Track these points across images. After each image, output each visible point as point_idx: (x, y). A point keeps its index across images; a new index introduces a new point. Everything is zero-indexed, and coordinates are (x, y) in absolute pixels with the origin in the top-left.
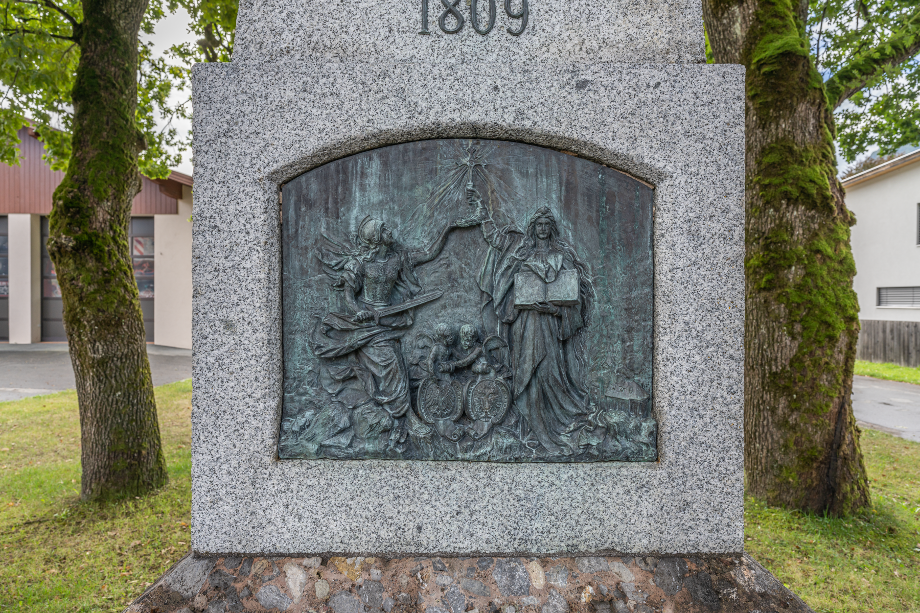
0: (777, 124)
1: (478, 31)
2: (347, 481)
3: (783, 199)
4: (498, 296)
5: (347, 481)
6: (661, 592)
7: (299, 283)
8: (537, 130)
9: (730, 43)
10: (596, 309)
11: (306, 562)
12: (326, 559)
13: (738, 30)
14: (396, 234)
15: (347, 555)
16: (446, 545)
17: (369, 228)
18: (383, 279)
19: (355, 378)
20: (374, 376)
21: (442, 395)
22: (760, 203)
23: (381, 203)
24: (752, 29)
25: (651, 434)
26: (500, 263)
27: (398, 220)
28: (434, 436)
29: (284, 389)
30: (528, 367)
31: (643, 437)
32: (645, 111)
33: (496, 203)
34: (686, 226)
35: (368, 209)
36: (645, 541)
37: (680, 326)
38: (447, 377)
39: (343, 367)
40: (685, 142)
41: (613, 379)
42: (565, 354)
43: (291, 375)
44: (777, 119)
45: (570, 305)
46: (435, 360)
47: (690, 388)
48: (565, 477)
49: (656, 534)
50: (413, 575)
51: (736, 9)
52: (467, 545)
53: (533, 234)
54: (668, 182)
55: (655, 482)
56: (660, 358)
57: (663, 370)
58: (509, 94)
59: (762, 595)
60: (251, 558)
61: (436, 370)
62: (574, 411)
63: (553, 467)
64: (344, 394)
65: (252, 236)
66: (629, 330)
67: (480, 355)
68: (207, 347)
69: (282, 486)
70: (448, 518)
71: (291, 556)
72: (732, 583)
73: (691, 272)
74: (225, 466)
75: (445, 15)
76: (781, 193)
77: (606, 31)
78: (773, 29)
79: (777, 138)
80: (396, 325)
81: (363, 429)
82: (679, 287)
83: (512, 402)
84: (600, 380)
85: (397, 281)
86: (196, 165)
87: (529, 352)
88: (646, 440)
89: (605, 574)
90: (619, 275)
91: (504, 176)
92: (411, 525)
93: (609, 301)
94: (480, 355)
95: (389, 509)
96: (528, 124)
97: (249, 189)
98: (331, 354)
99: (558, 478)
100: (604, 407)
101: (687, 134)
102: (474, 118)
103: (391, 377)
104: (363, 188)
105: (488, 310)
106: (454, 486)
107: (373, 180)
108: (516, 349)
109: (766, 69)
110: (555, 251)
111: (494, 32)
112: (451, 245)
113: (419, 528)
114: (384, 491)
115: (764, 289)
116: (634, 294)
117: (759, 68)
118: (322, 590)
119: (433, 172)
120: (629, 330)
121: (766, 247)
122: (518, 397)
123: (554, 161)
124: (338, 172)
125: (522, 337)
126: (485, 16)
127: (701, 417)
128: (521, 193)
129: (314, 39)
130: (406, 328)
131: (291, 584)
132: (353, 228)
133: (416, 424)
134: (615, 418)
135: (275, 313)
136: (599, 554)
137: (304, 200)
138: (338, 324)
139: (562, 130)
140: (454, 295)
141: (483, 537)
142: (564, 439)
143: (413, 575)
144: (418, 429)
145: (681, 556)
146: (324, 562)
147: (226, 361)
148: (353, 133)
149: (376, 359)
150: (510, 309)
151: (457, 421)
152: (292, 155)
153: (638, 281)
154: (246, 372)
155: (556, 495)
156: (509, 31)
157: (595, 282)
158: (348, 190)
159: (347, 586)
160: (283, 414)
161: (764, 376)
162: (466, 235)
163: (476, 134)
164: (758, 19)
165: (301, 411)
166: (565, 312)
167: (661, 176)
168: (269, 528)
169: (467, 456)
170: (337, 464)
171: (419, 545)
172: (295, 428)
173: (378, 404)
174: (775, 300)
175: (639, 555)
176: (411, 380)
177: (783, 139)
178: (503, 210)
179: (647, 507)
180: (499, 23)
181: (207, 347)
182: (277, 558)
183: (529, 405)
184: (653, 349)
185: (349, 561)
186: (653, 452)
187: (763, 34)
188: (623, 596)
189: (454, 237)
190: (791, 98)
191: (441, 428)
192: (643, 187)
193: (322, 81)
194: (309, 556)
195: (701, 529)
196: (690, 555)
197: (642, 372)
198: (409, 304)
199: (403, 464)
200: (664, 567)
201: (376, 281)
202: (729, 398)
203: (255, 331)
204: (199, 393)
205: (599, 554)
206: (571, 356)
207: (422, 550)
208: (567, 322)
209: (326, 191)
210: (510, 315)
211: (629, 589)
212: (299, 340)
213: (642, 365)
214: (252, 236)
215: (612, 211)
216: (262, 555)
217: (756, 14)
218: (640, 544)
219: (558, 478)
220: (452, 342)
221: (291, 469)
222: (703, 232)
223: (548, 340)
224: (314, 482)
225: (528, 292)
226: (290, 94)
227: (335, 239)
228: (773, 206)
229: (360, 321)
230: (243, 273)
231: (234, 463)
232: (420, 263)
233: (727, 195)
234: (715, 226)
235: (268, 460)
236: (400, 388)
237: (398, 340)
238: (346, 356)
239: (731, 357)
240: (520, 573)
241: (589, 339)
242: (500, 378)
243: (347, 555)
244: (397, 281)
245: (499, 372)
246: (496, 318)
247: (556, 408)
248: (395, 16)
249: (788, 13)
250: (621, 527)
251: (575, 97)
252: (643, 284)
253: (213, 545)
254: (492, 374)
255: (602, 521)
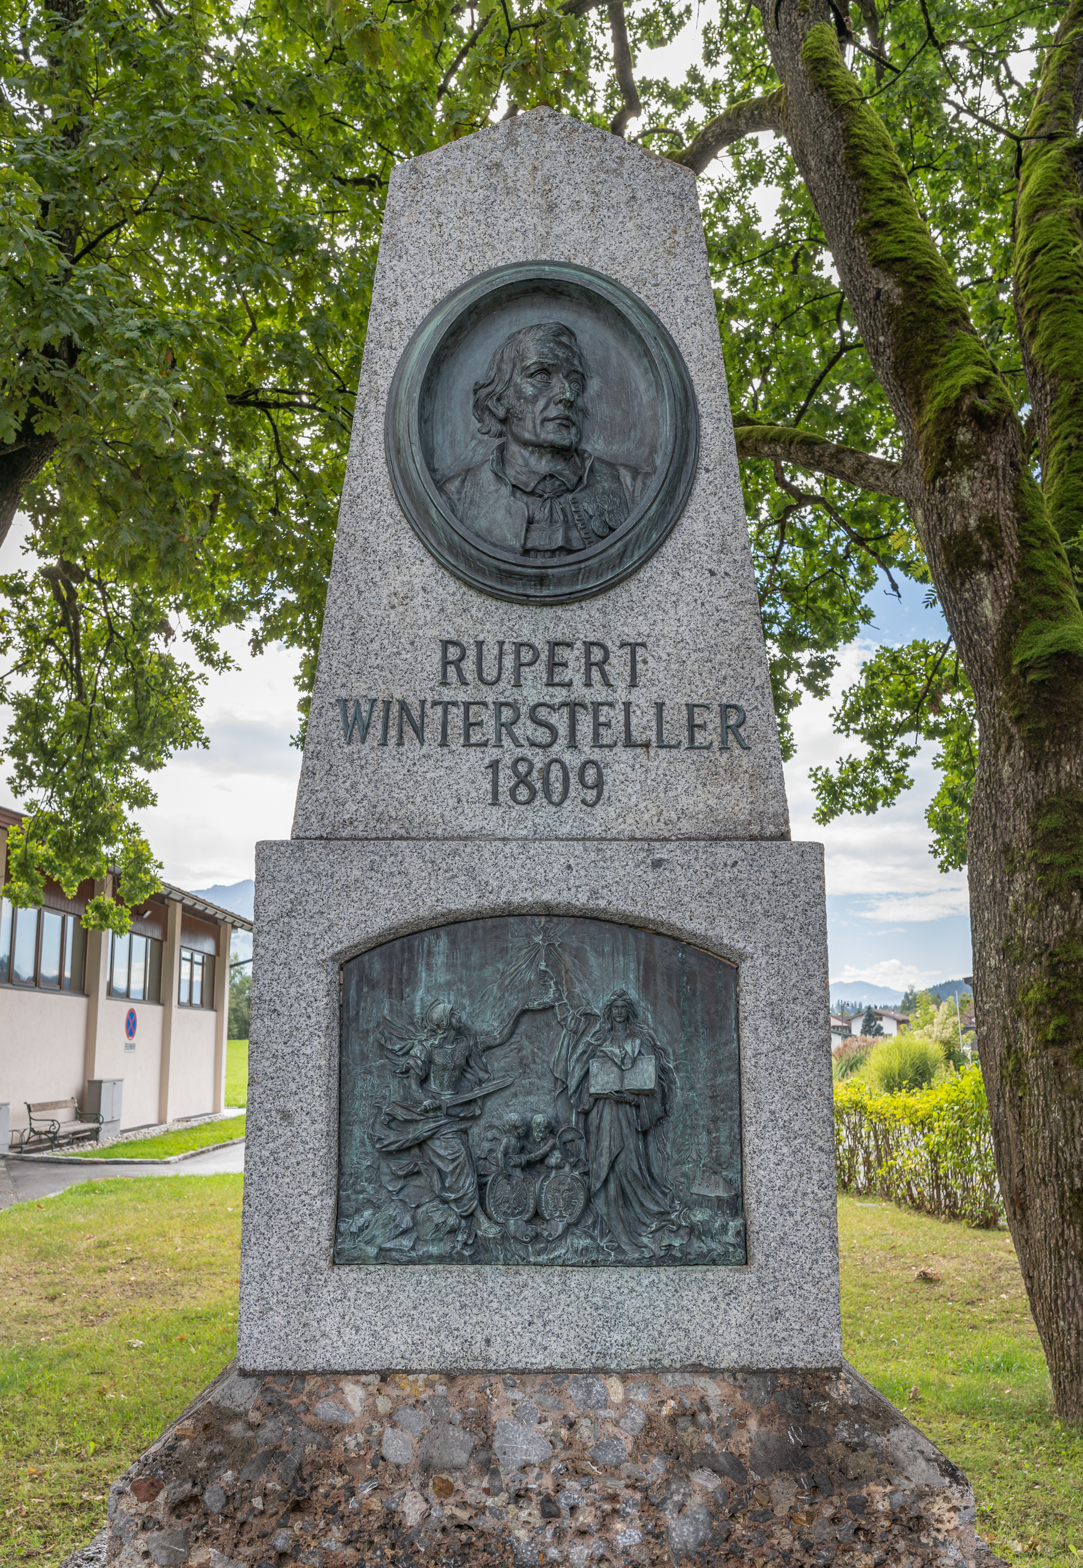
0: (1058, 766)
1: (551, 802)
2: (409, 1288)
3: (1073, 889)
4: (573, 1083)
5: (409, 1288)
6: (748, 1406)
7: (358, 1069)
8: (612, 909)
9: (976, 629)
10: (679, 1097)
11: (363, 1378)
12: (385, 1375)
13: (989, 611)
14: (464, 1017)
15: (408, 1372)
16: (516, 1360)
17: (440, 1010)
18: (451, 1065)
19: (418, 1173)
20: (439, 1170)
21: (513, 1191)
22: (1039, 895)
23: (449, 984)
24: (1010, 611)
25: (738, 1233)
26: (575, 1047)
27: (466, 1002)
28: (504, 1237)
29: (339, 1187)
30: (605, 1160)
31: (730, 1238)
32: (723, 890)
33: (571, 984)
34: (768, 1010)
35: (434, 994)
36: (734, 1355)
37: (766, 1116)
38: (518, 1172)
39: (403, 1164)
40: (765, 922)
41: (699, 1174)
42: (646, 1147)
43: (347, 1170)
44: (1057, 756)
45: (649, 1094)
46: (506, 1154)
47: (778, 1183)
48: (646, 1282)
49: (746, 1346)
50: (482, 1390)
51: (982, 577)
52: (540, 1361)
53: (609, 1017)
54: (749, 963)
55: (744, 1288)
56: (746, 1150)
57: (751, 1163)
58: (583, 873)
59: (854, 1407)
60: (303, 1375)
61: (506, 1164)
62: (655, 1209)
63: (633, 1271)
64: (406, 1191)
65: (313, 1020)
66: (715, 1120)
67: (553, 1148)
68: (262, 1140)
69: (338, 1294)
70: (519, 1329)
71: (346, 1373)
72: (825, 1397)
73: (775, 1058)
74: (277, 1272)
75: (517, 785)
76: (1069, 879)
77: (684, 801)
78: (1044, 612)
79: (1059, 788)
80: (464, 1115)
81: (428, 1230)
82: (763, 1073)
83: (589, 1201)
84: (685, 1175)
85: (464, 1068)
86: (256, 946)
87: (606, 1144)
88: (732, 1240)
89: (688, 1388)
90: (703, 1060)
91: (579, 955)
92: (479, 1337)
93: (692, 1088)
94: (553, 1148)
95: (455, 1320)
96: (602, 903)
97: (312, 971)
98: (393, 1147)
99: (639, 1283)
100: (688, 1206)
101: (766, 914)
102: (546, 897)
103: (458, 1172)
104: (429, 967)
105: (563, 1098)
106: (526, 1293)
107: (440, 960)
108: (593, 1141)
109: (1032, 677)
110: (632, 1035)
111: (568, 802)
112: (523, 1027)
113: (488, 1341)
114: (449, 1299)
115: (1053, 1041)
116: (719, 1081)
117: (1024, 673)
118: (383, 1405)
119: (504, 951)
120: (715, 1120)
121: (1053, 970)
122: (595, 1195)
123: (631, 939)
124: (403, 951)
125: (599, 1128)
126: (558, 786)
127: (791, 1214)
128: (596, 973)
129: (379, 809)
130: (474, 1118)
131: (349, 1399)
132: (418, 1010)
133: (485, 1224)
134: (699, 1216)
135: (334, 1103)
136: (684, 1369)
137: (366, 980)
138: (401, 1114)
139: (637, 910)
140: (525, 1082)
141: (558, 1351)
142: (645, 1240)
143: (482, 1390)
144: (487, 1229)
145: (774, 1372)
146: (383, 1379)
147: (282, 1155)
148: (421, 913)
149: (442, 1152)
150: (585, 1098)
151: (529, 1222)
152: (358, 936)
153: (723, 1066)
154: (303, 1166)
155: (637, 1302)
156: (584, 802)
157: (676, 1067)
158: (413, 970)
159: (411, 1401)
160: (339, 1214)
161: (1062, 1198)
162: (538, 1017)
163: (549, 912)
164: (1017, 594)
165: (358, 1211)
166: (643, 1101)
167: (743, 957)
168: (323, 1342)
169: (540, 1259)
170: (398, 1269)
171: (487, 1360)
172: (354, 1229)
173: (445, 1202)
174: (1071, 1061)
175: (727, 1370)
176: (480, 1176)
177: (1068, 790)
178: (577, 990)
179: (736, 1316)
180: (572, 794)
181: (262, 1140)
182: (333, 1375)
183: (607, 1203)
184: (740, 1141)
185: (411, 1378)
186: (741, 1254)
187: (1027, 619)
188: (708, 1410)
189: (525, 1019)
190: (1077, 724)
191: (512, 1228)
192: (726, 966)
193: (390, 860)
194: (366, 1373)
195: (795, 1341)
196: (784, 1371)
197: (730, 1166)
198: (477, 1092)
199: (471, 1269)
200: (754, 1381)
201: (444, 1068)
202: (821, 1194)
203: (314, 1122)
204: (252, 1189)
205: (684, 1369)
206: (652, 1149)
207: (490, 1366)
208: (648, 1112)
209: (390, 970)
210: (587, 1104)
211: (712, 1403)
212: (357, 1131)
213: (730, 1159)
214: (313, 1020)
215: (694, 991)
216: (314, 1372)
217: (1014, 586)
218: (728, 1359)
219: (639, 1283)
220: (524, 1133)
221: (349, 1274)
222: (786, 1016)
223: (626, 1131)
224: (373, 1289)
225: (603, 1080)
226: (357, 873)
227: (399, 1023)
228: (1059, 901)
229: (426, 1111)
230: (303, 1059)
231: (287, 1268)
232: (490, 1048)
233: (810, 977)
234: (800, 1010)
235: (324, 1264)
236: (468, 1183)
237: (465, 1132)
238: (409, 1149)
239: (821, 1149)
240: (598, 1387)
241: (672, 1129)
242: (576, 1173)
243: (408, 1372)
244: (464, 1068)
245: (574, 1166)
246: (571, 1107)
247: (636, 1206)
248: (465, 786)
249: (1067, 587)
250: (709, 1339)
251: (651, 876)
252: (729, 1069)
253: (260, 1362)
254: (567, 1168)
255: (687, 1331)
